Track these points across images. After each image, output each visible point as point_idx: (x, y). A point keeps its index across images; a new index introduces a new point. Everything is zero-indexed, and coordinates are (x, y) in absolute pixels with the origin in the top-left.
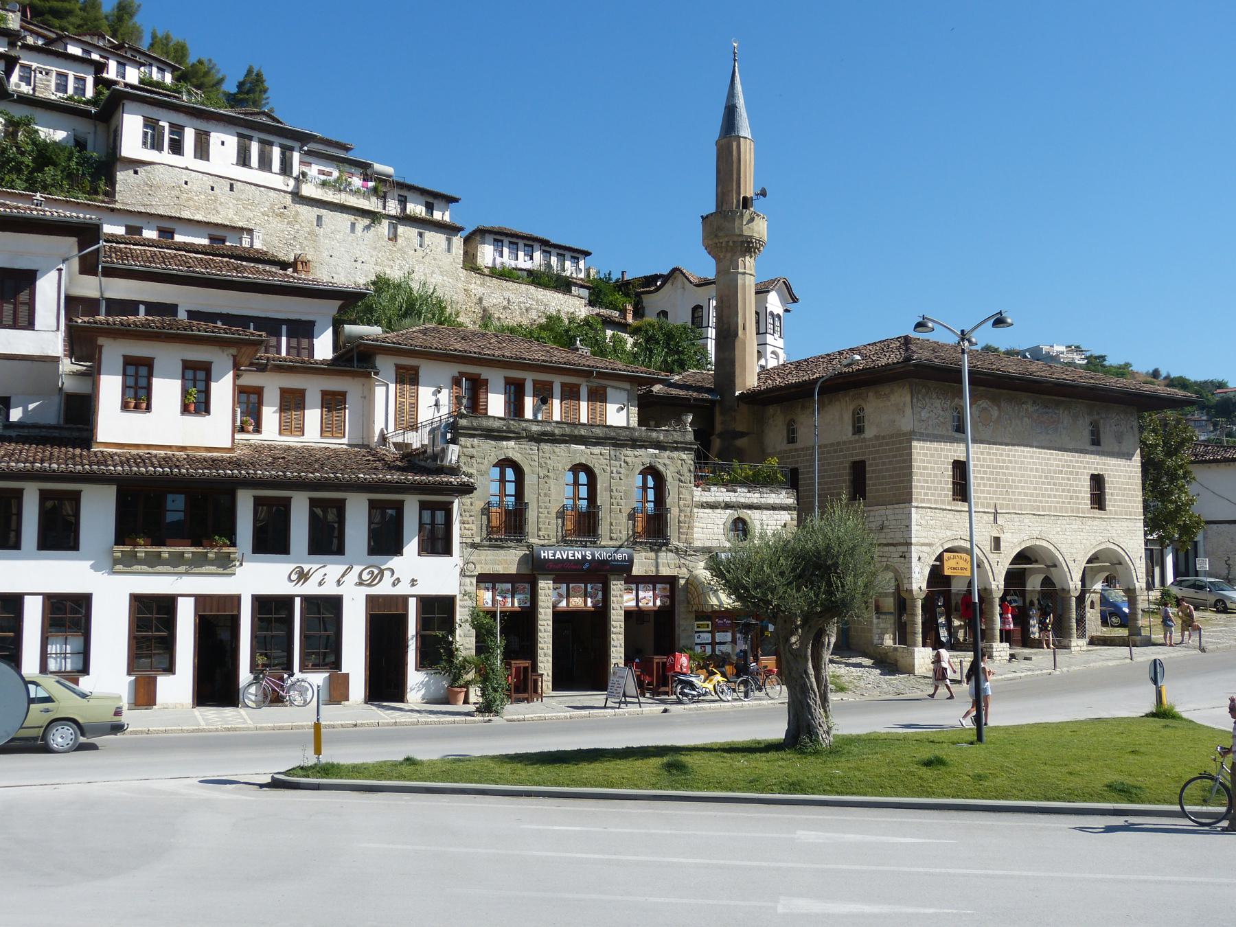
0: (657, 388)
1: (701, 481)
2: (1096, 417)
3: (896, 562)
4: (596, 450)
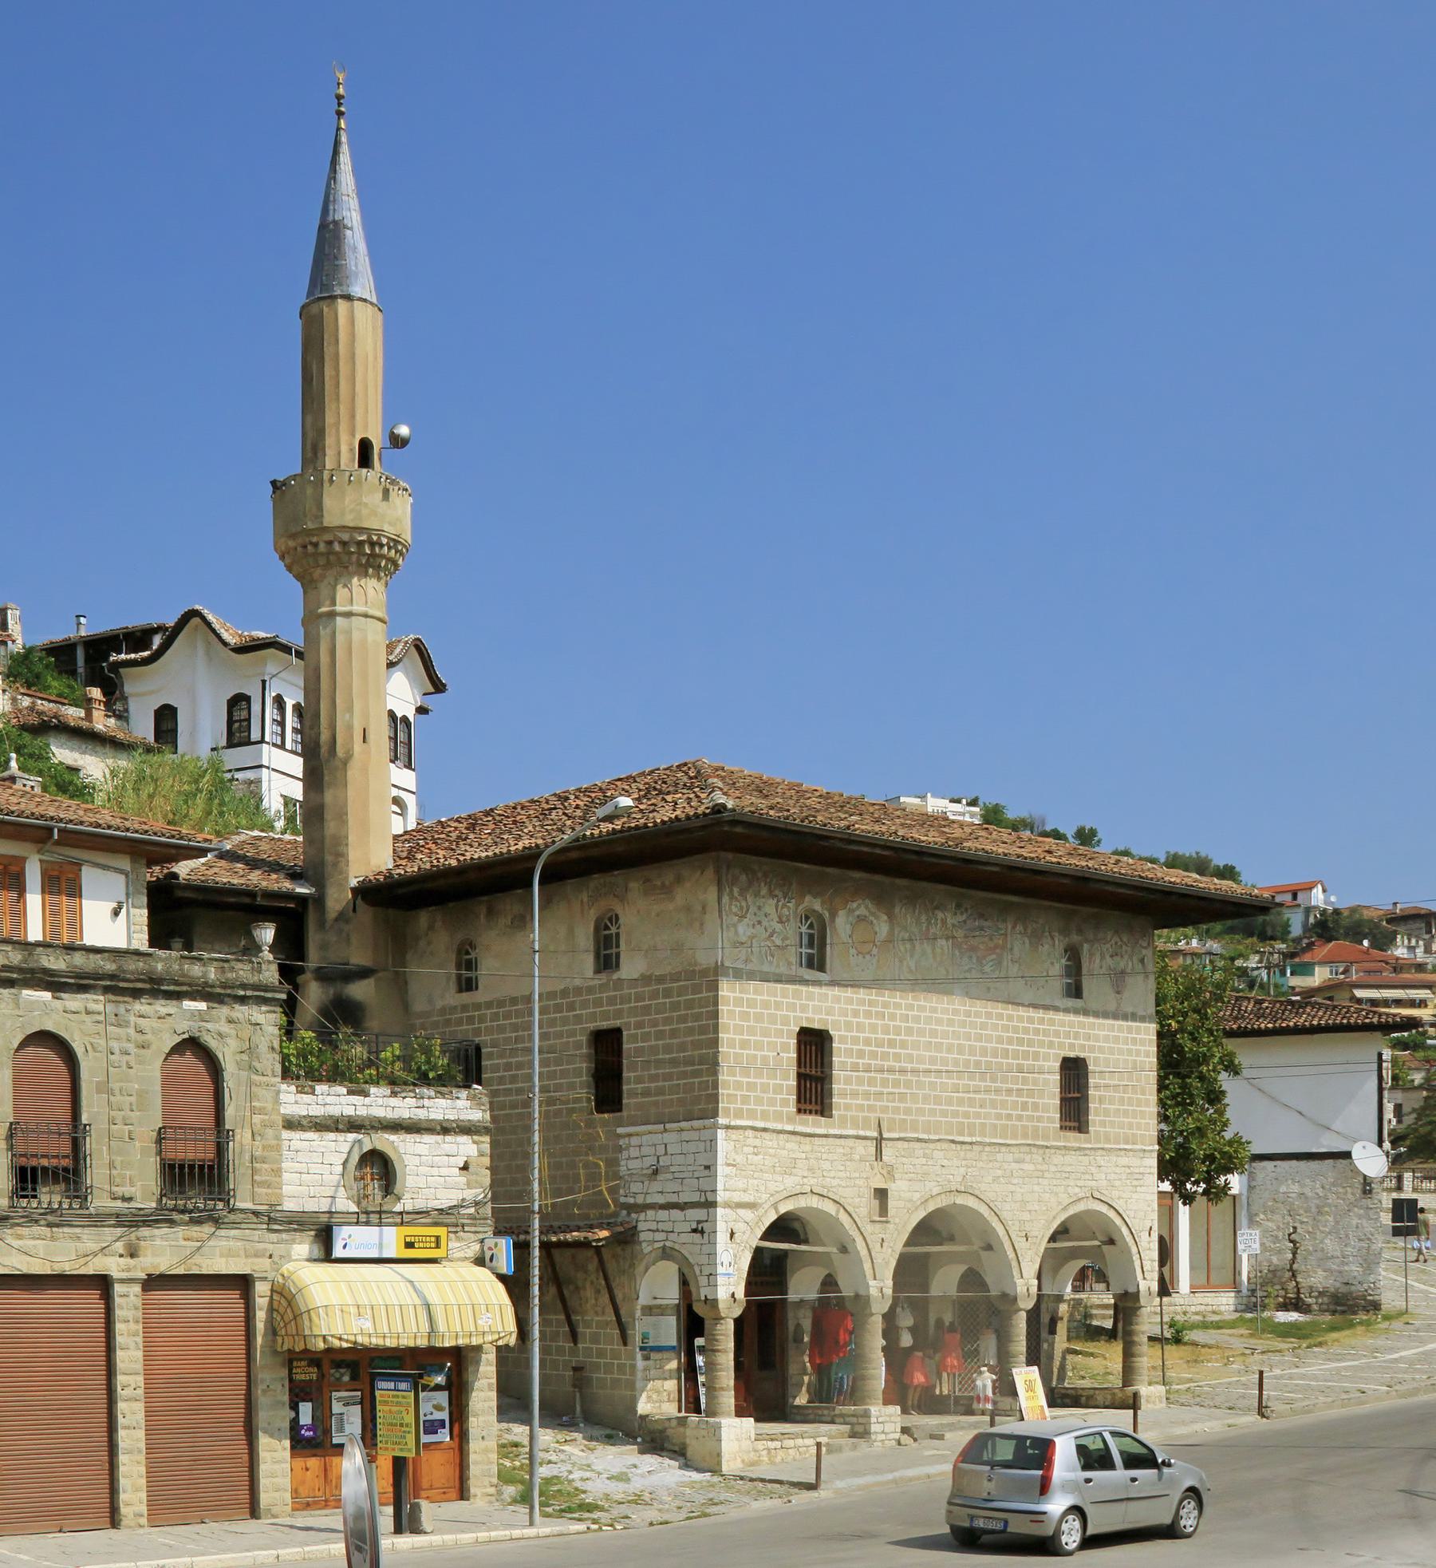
0: (183, 869)
1: (301, 1070)
2: (1075, 938)
3: (685, 1242)
4: (74, 1001)
